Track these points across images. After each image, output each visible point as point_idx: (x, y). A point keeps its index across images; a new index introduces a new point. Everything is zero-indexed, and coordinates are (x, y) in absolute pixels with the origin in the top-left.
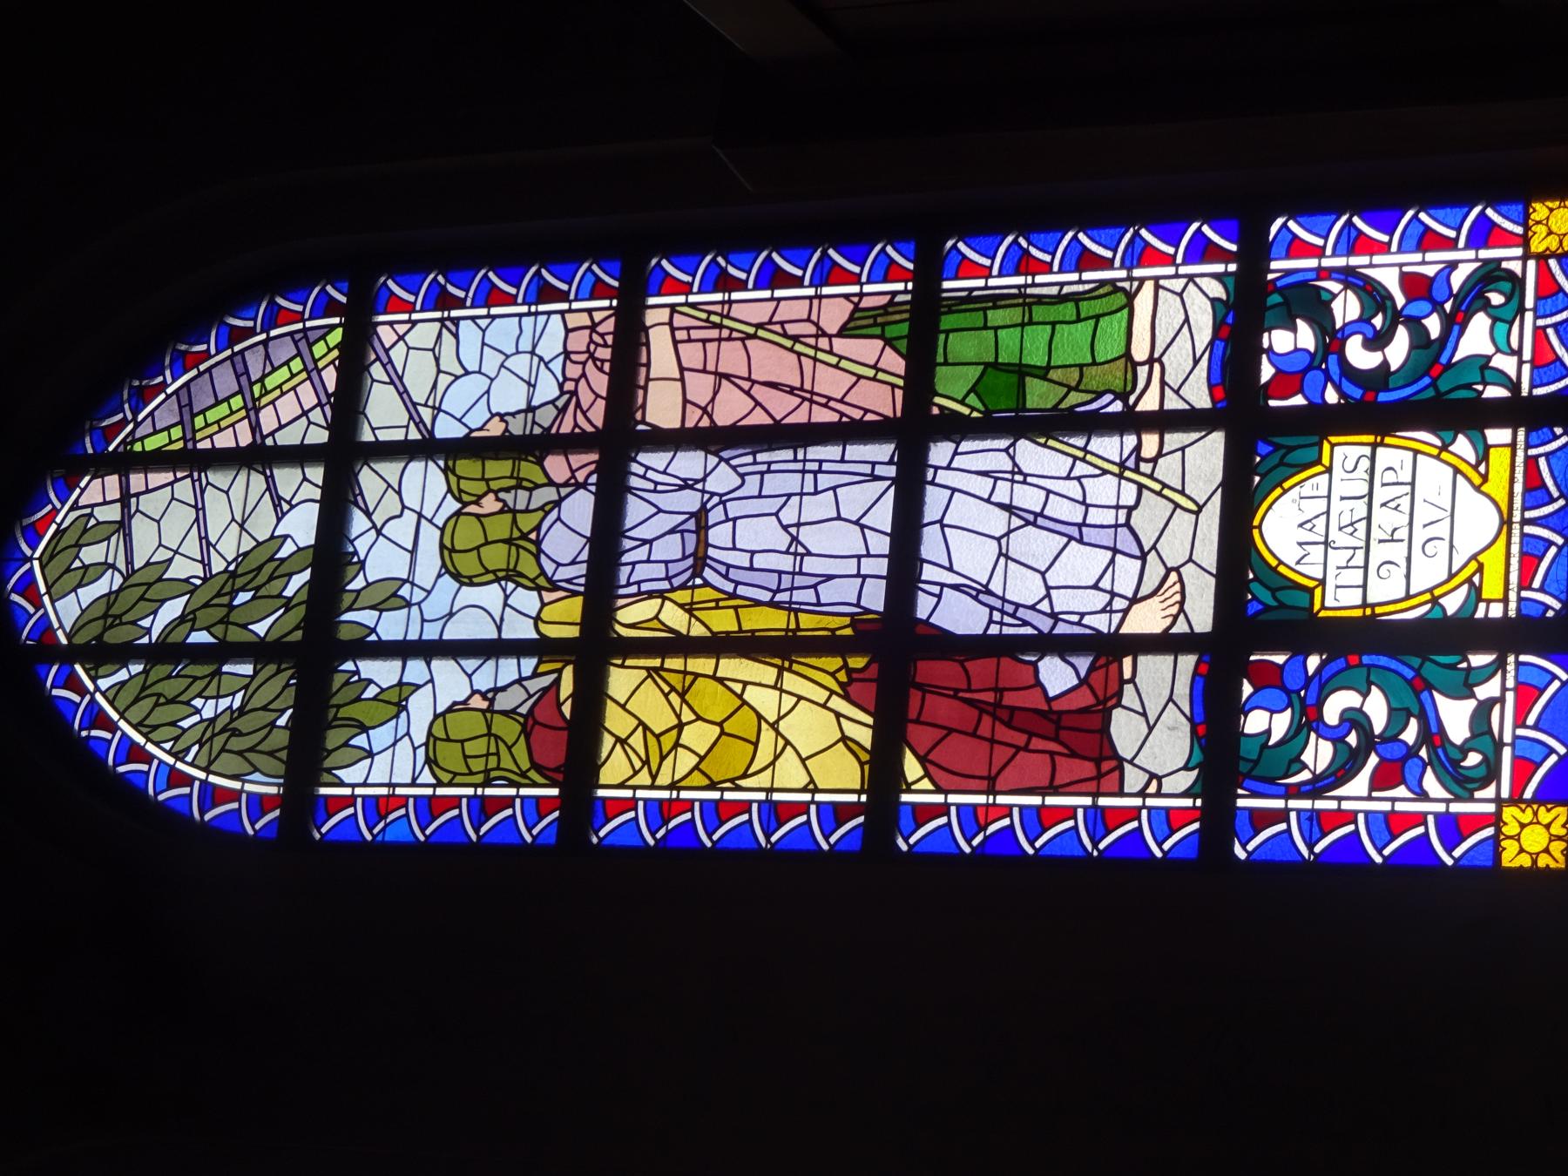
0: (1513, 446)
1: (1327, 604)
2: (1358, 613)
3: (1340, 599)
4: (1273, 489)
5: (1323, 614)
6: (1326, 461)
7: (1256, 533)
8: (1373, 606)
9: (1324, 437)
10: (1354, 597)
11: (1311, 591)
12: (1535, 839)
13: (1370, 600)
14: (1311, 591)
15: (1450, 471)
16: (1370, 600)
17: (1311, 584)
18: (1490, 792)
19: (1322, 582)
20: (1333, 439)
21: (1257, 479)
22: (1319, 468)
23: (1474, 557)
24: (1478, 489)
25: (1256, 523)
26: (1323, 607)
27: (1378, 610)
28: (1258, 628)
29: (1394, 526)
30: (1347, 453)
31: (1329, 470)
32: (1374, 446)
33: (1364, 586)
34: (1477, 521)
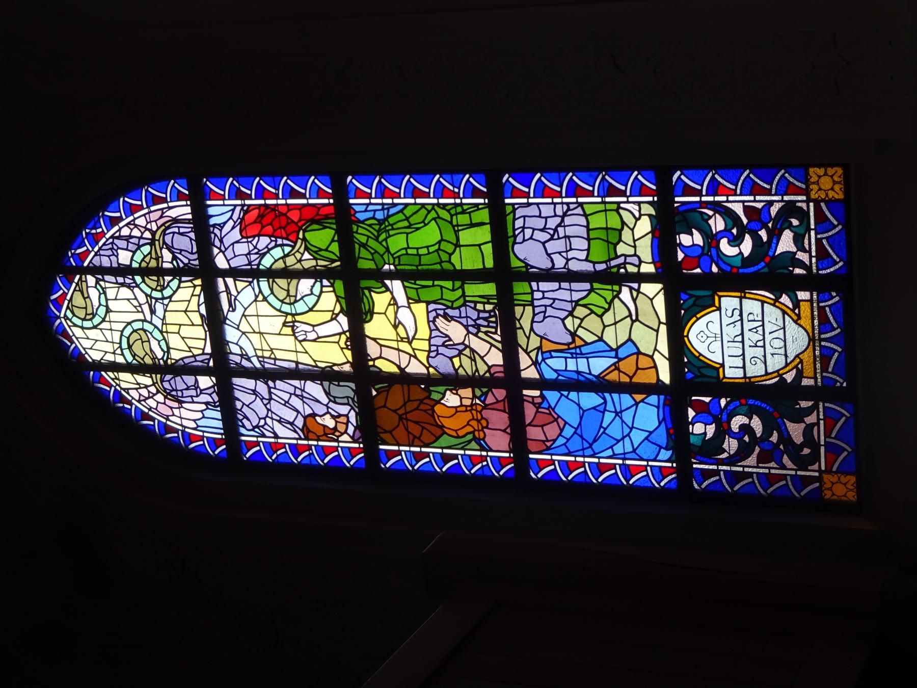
1: (722, 299)
3: (732, 373)
6: (717, 304)
8: (750, 378)
9: (714, 293)
10: (739, 373)
11: (718, 369)
13: (748, 375)
14: (718, 369)
16: (748, 375)
17: (718, 366)
18: (816, 467)
19: (723, 365)
20: (720, 294)
22: (714, 308)
23: (797, 356)
24: (796, 322)
25: (685, 334)
26: (724, 377)
28: (693, 380)
30: (729, 302)
31: (719, 309)
32: (741, 298)
33: (744, 367)
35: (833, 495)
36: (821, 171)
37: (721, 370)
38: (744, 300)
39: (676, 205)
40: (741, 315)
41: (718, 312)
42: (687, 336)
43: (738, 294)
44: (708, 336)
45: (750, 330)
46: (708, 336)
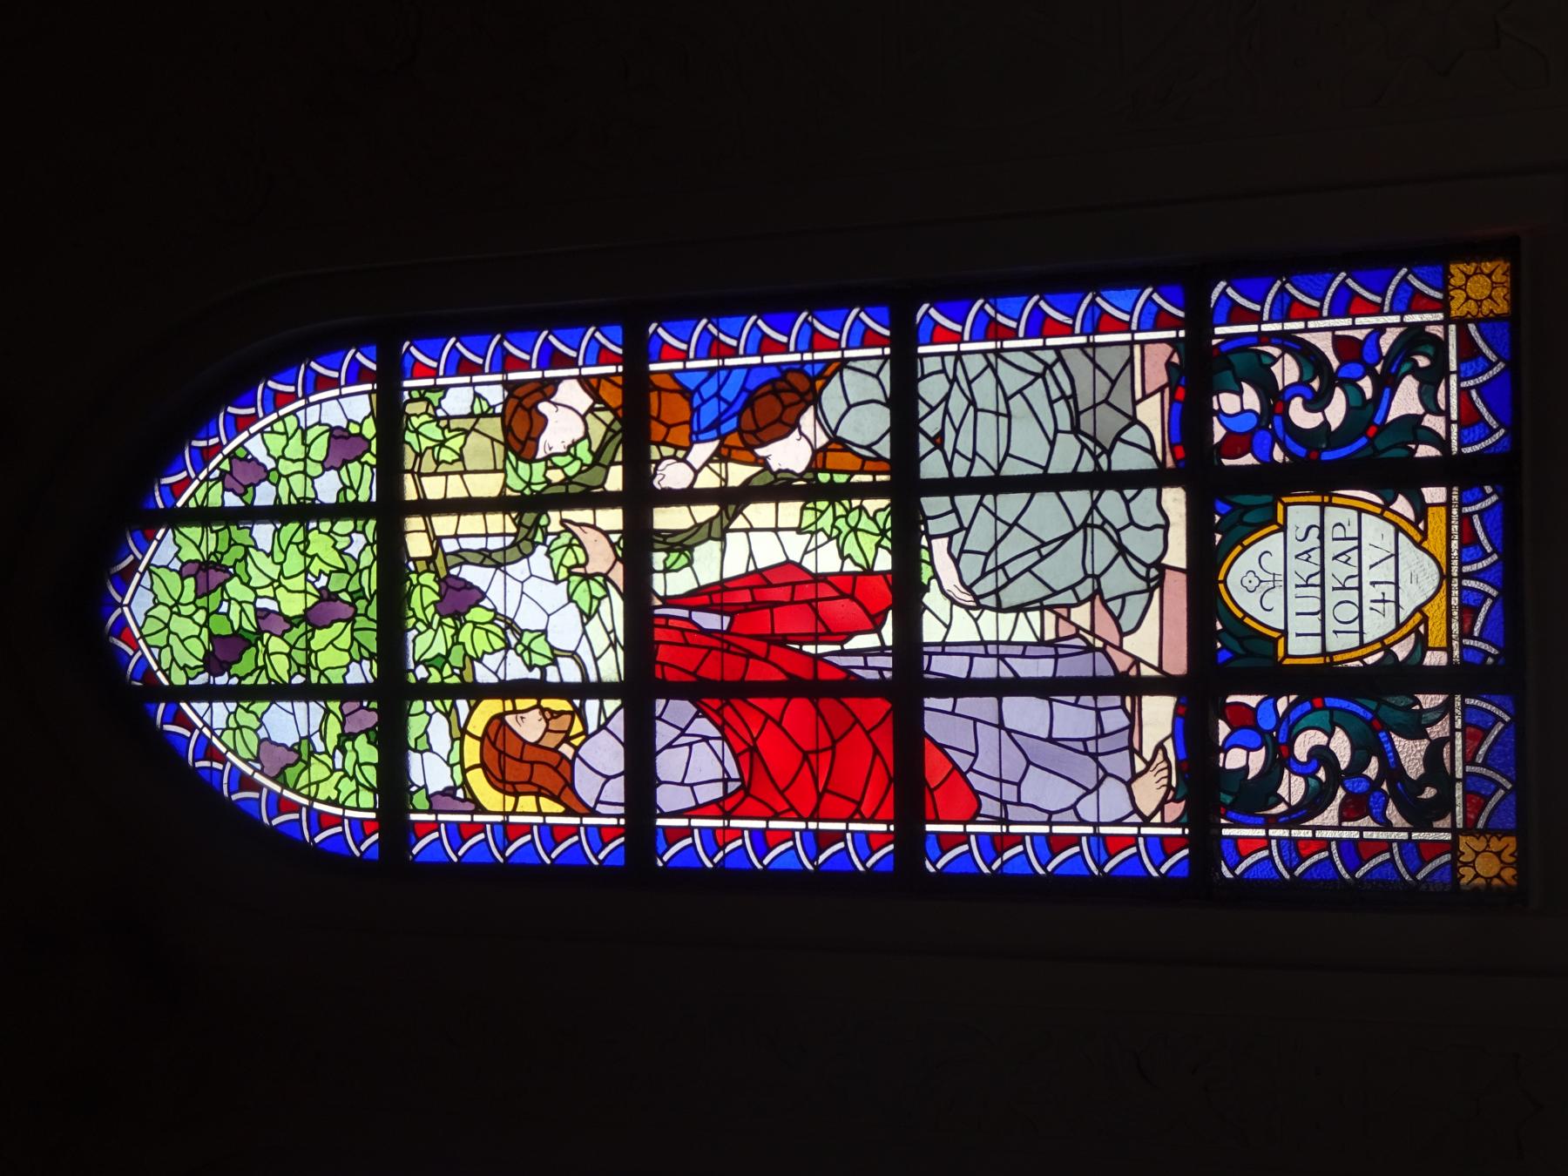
0: (1448, 505)
2: (1320, 661)
3: (1302, 647)
4: (1049, 554)
5: (1287, 662)
6: (1280, 520)
7: (1221, 586)
9: (1278, 499)
10: (1313, 646)
12: (1487, 866)
14: (1275, 641)
15: (1392, 528)
17: (1275, 635)
19: (1284, 633)
20: (1286, 500)
21: (1218, 537)
22: (1275, 527)
23: (1419, 609)
24: (1418, 545)
25: (1221, 577)
26: (1287, 655)
27: (1337, 658)
28: (1227, 662)
29: (1353, 578)
30: (1301, 515)
31: (1283, 528)
32: (1322, 506)
33: (1323, 634)
34: (1420, 578)
35: (1477, 875)
36: (1470, 269)
37: (1281, 642)
38: (1328, 510)
39: (1215, 342)
40: (1321, 537)
41: (1281, 534)
42: (1224, 582)
43: (1318, 499)
44: (1260, 580)
45: (1335, 558)
46: (1260, 580)
